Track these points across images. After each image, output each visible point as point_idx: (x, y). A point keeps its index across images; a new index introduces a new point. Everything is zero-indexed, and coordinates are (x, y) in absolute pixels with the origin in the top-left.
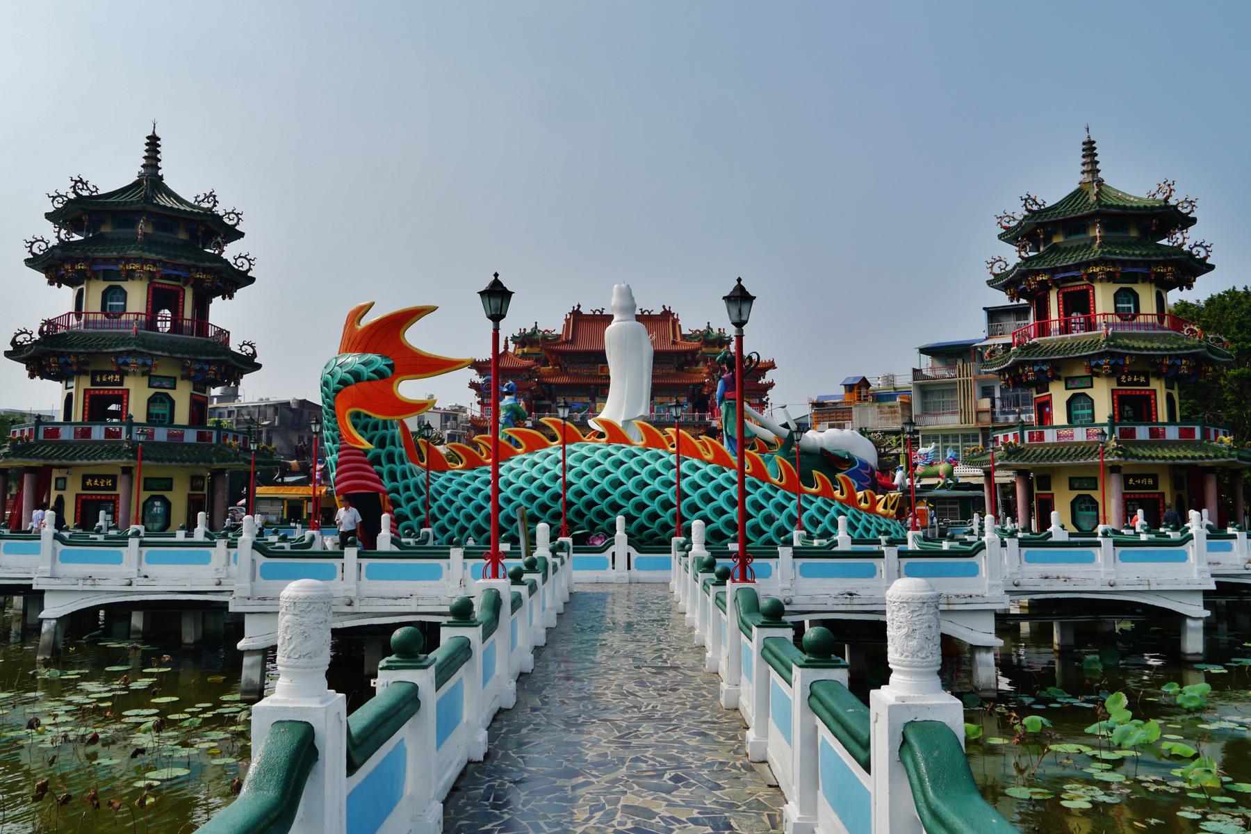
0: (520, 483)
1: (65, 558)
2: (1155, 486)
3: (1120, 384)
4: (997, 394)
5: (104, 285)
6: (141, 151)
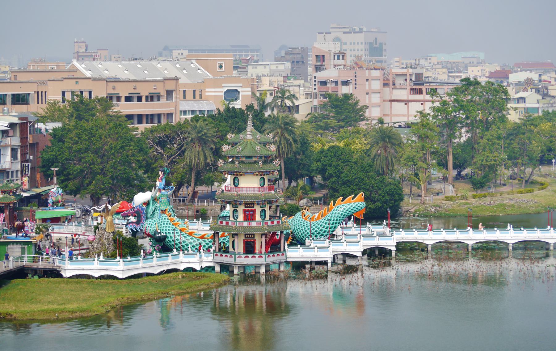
3: (245, 207)
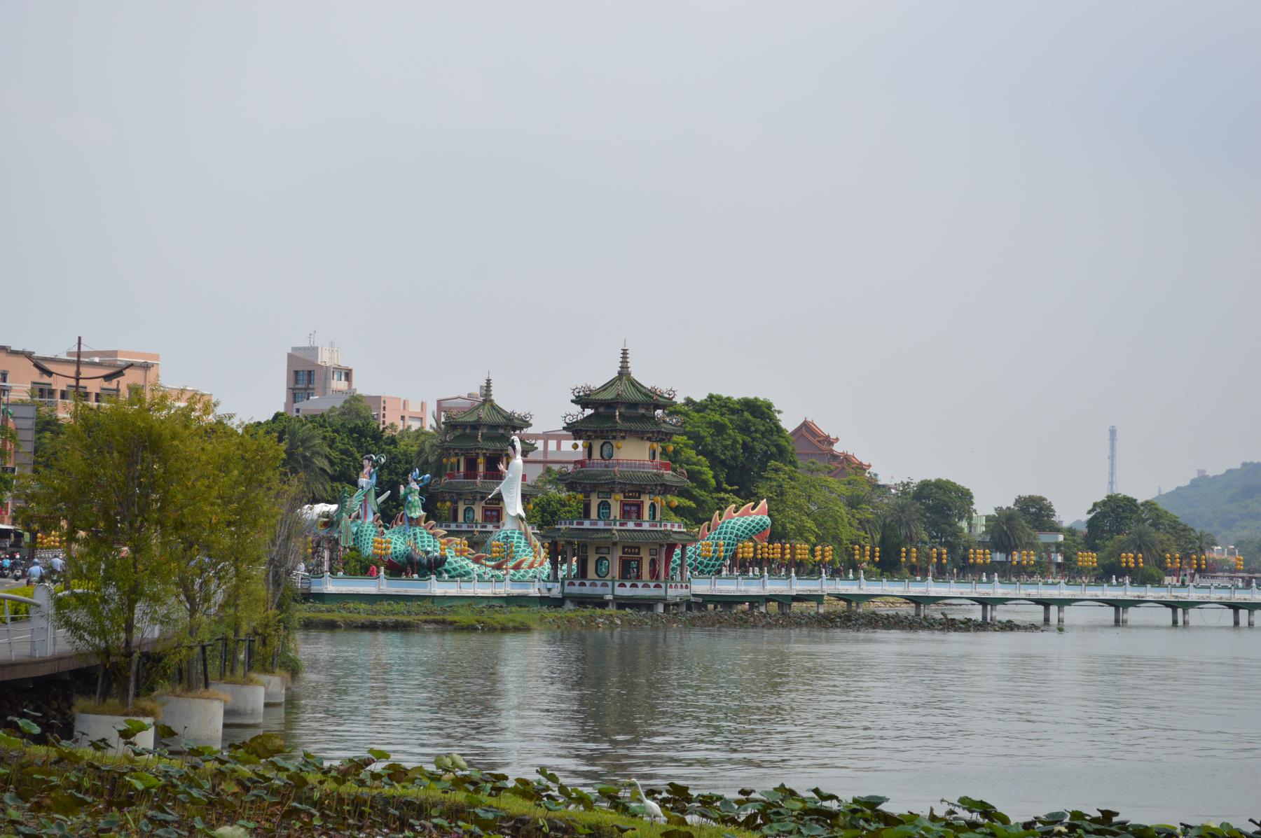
5: (601, 442)
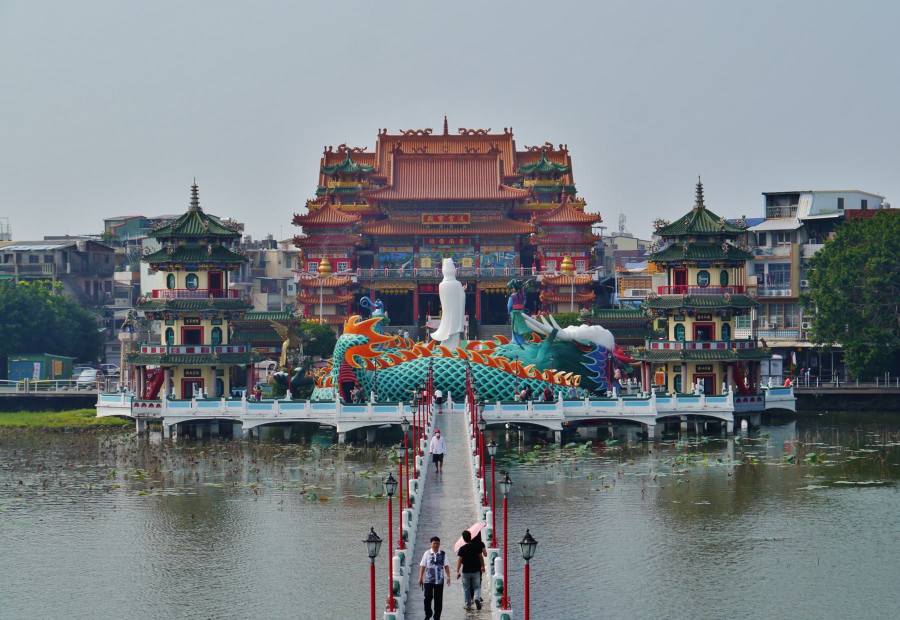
0: (406, 375)
1: (250, 408)
2: (711, 371)
4: (766, 272)
5: (187, 273)
6: (189, 194)
